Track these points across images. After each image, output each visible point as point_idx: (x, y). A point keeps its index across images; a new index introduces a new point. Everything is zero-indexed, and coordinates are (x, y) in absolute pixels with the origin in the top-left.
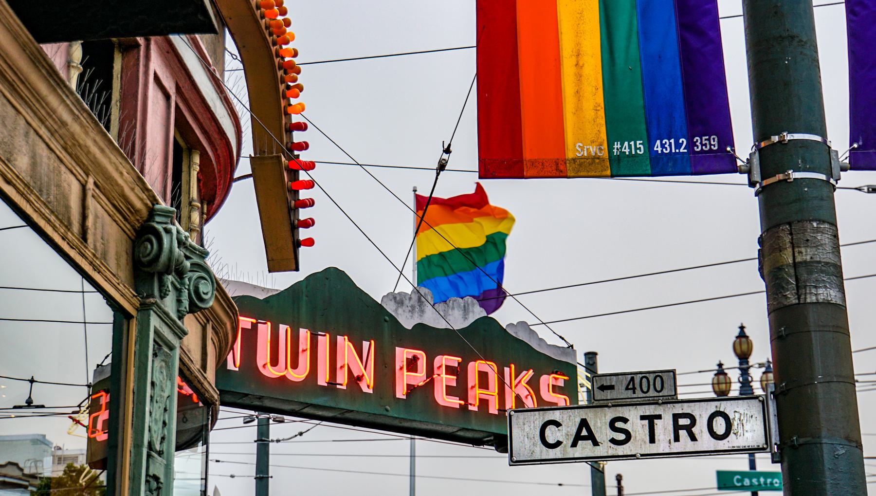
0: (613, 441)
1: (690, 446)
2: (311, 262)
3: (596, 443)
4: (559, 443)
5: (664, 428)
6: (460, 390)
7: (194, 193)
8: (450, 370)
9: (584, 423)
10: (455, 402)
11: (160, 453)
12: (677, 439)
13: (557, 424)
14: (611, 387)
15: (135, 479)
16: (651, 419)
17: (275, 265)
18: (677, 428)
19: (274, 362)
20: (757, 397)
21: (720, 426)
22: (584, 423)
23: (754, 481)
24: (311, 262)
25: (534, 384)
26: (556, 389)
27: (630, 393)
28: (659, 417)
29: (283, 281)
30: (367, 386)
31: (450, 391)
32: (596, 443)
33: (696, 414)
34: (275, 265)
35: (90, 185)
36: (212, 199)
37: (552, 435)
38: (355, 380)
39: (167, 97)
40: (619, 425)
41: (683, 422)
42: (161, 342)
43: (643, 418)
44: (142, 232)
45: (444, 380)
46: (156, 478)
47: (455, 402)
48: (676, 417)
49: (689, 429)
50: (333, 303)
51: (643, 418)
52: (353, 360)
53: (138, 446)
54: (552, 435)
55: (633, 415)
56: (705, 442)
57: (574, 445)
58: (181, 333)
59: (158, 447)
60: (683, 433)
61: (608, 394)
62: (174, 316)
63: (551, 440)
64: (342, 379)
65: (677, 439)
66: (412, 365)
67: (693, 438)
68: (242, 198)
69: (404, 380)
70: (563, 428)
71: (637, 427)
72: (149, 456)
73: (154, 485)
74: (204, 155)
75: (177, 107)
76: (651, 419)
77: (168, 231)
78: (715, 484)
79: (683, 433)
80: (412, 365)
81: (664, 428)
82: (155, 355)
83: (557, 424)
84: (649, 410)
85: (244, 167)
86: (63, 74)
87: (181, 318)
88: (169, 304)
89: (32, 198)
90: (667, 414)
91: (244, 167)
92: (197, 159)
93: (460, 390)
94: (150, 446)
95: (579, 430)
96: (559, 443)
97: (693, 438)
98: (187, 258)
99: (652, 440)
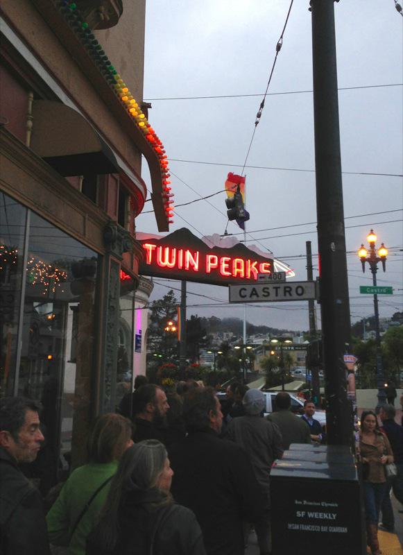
0: (264, 296)
1: (290, 298)
2: (173, 228)
3: (258, 296)
4: (245, 296)
5: (281, 292)
6: (230, 269)
7: (129, 209)
8: (226, 262)
9: (254, 289)
10: (228, 274)
11: (114, 299)
12: (285, 295)
13: (245, 289)
14: (263, 277)
15: (105, 307)
16: (277, 288)
17: (161, 230)
18: (285, 291)
19: (163, 260)
20: (313, 281)
21: (300, 291)
22: (254, 289)
23: (376, 291)
24: (173, 228)
25: (257, 267)
26: (265, 268)
27: (270, 280)
28: (279, 288)
29: (165, 234)
30: (196, 267)
31: (226, 270)
32: (258, 296)
33: (292, 287)
34: (161, 230)
35: (87, 217)
36: (138, 209)
37: (243, 293)
38: (192, 266)
39: (116, 181)
40: (266, 290)
41: (287, 289)
42: (114, 263)
43: (274, 288)
44: (106, 228)
45: (224, 266)
46: (113, 307)
47: (228, 274)
48: (285, 288)
49: (289, 292)
50: (184, 239)
51: (274, 288)
52: (190, 259)
53: (106, 297)
54: (243, 293)
55: (270, 286)
56: (295, 296)
57: (251, 297)
58: (121, 259)
59: (113, 297)
60: (287, 294)
61: (263, 280)
62: (118, 254)
63: (242, 294)
64: (188, 266)
65: (285, 295)
66: (213, 261)
67: (290, 295)
68: (149, 206)
69: (210, 266)
70: (247, 291)
71: (272, 291)
72: (110, 300)
73: (112, 309)
74: (132, 197)
75: (121, 183)
76: (277, 288)
77: (114, 229)
78: (359, 291)
79: (287, 294)
80: (213, 261)
81: (281, 292)
82: (111, 268)
83: (245, 289)
84: (275, 285)
85: (149, 197)
86: (77, 188)
87: (121, 254)
88: (116, 251)
89: (65, 225)
90: (282, 286)
91: (149, 197)
92: (130, 198)
93: (230, 269)
94: (110, 296)
95: (256, 292)
96: (245, 296)
97: (290, 295)
98: (123, 235)
99: (277, 295)
